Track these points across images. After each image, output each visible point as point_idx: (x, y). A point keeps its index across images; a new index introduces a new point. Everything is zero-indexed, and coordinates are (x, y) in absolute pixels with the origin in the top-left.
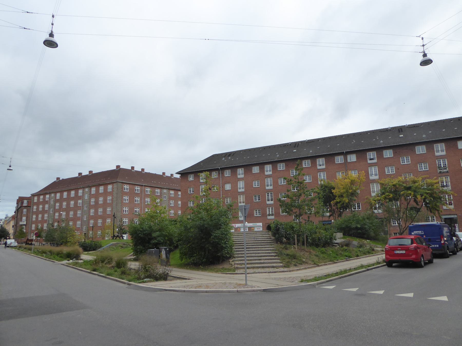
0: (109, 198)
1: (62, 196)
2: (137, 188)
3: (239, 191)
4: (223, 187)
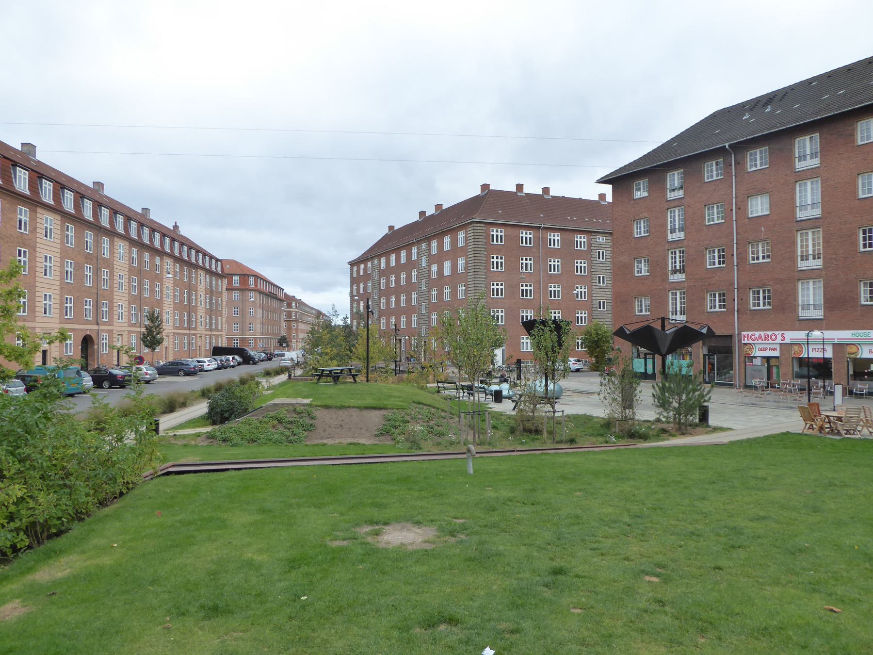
0: (461, 262)
2: (526, 234)
3: (801, 215)
4: (742, 208)
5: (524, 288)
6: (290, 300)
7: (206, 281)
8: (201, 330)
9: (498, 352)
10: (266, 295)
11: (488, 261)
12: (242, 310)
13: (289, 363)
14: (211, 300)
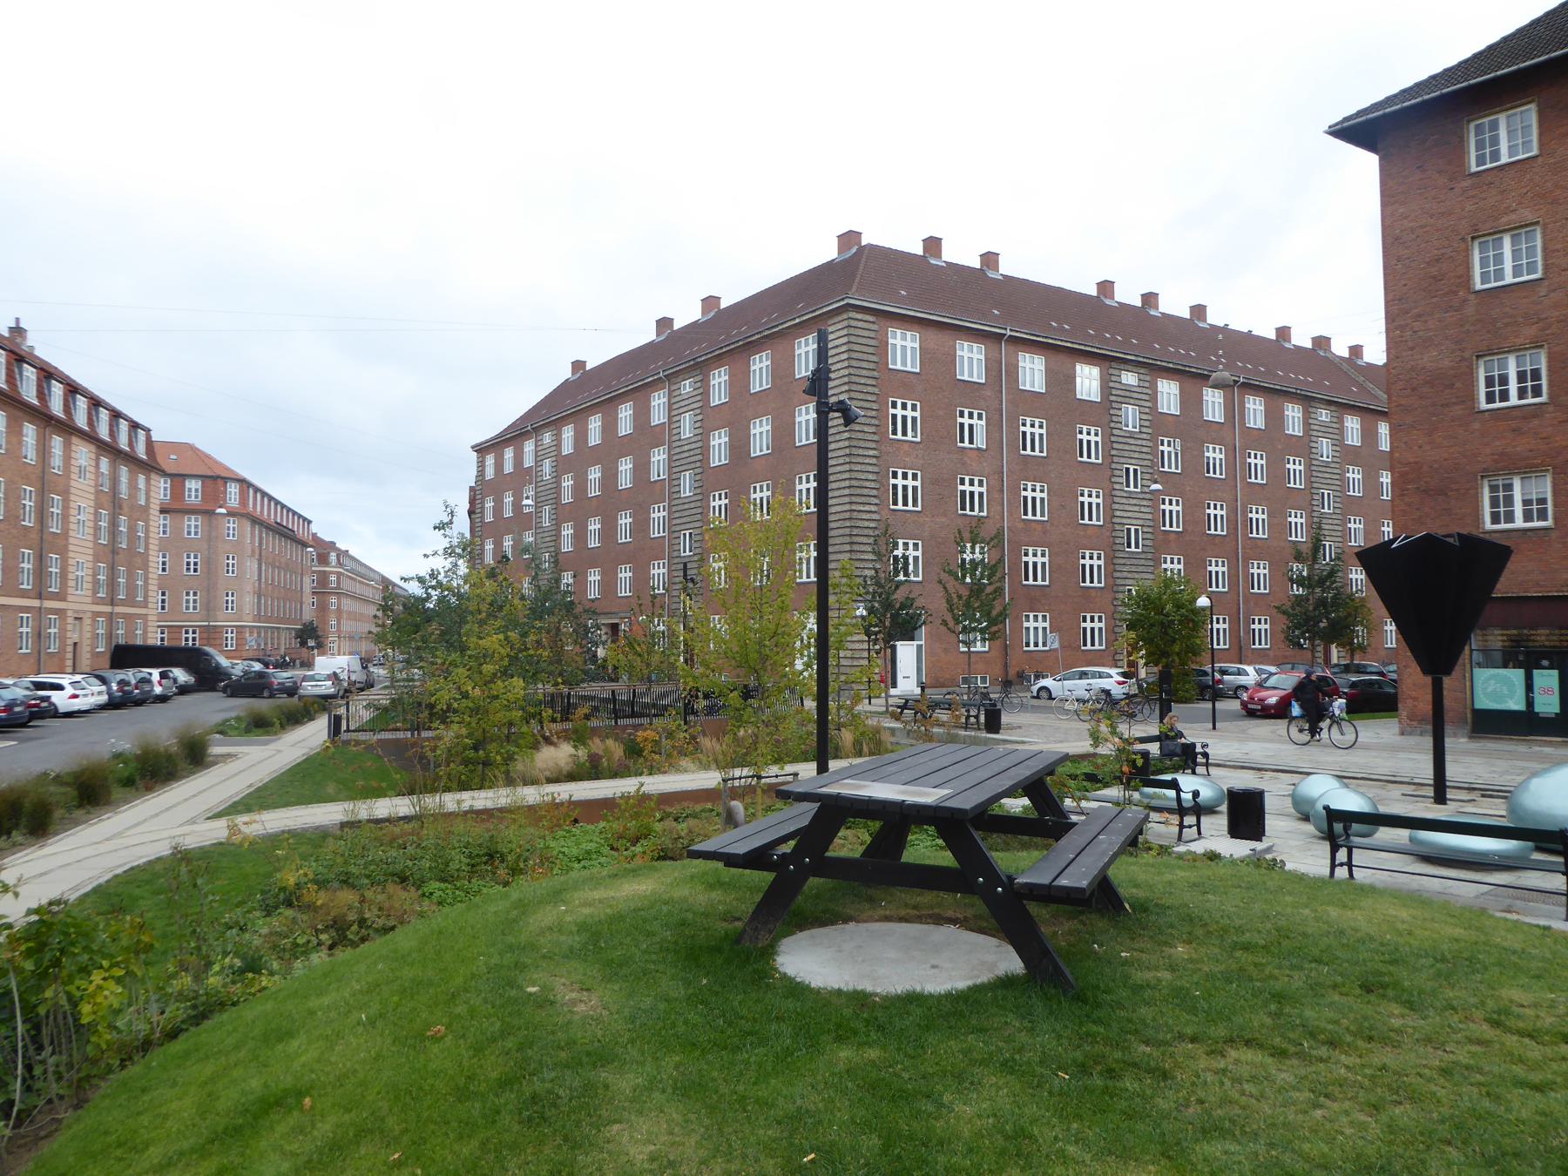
5: (967, 488)
6: (325, 549)
7: (98, 473)
8: (80, 599)
9: (906, 653)
10: (268, 527)
11: (882, 412)
12: (208, 562)
13: (327, 688)
14: (114, 524)
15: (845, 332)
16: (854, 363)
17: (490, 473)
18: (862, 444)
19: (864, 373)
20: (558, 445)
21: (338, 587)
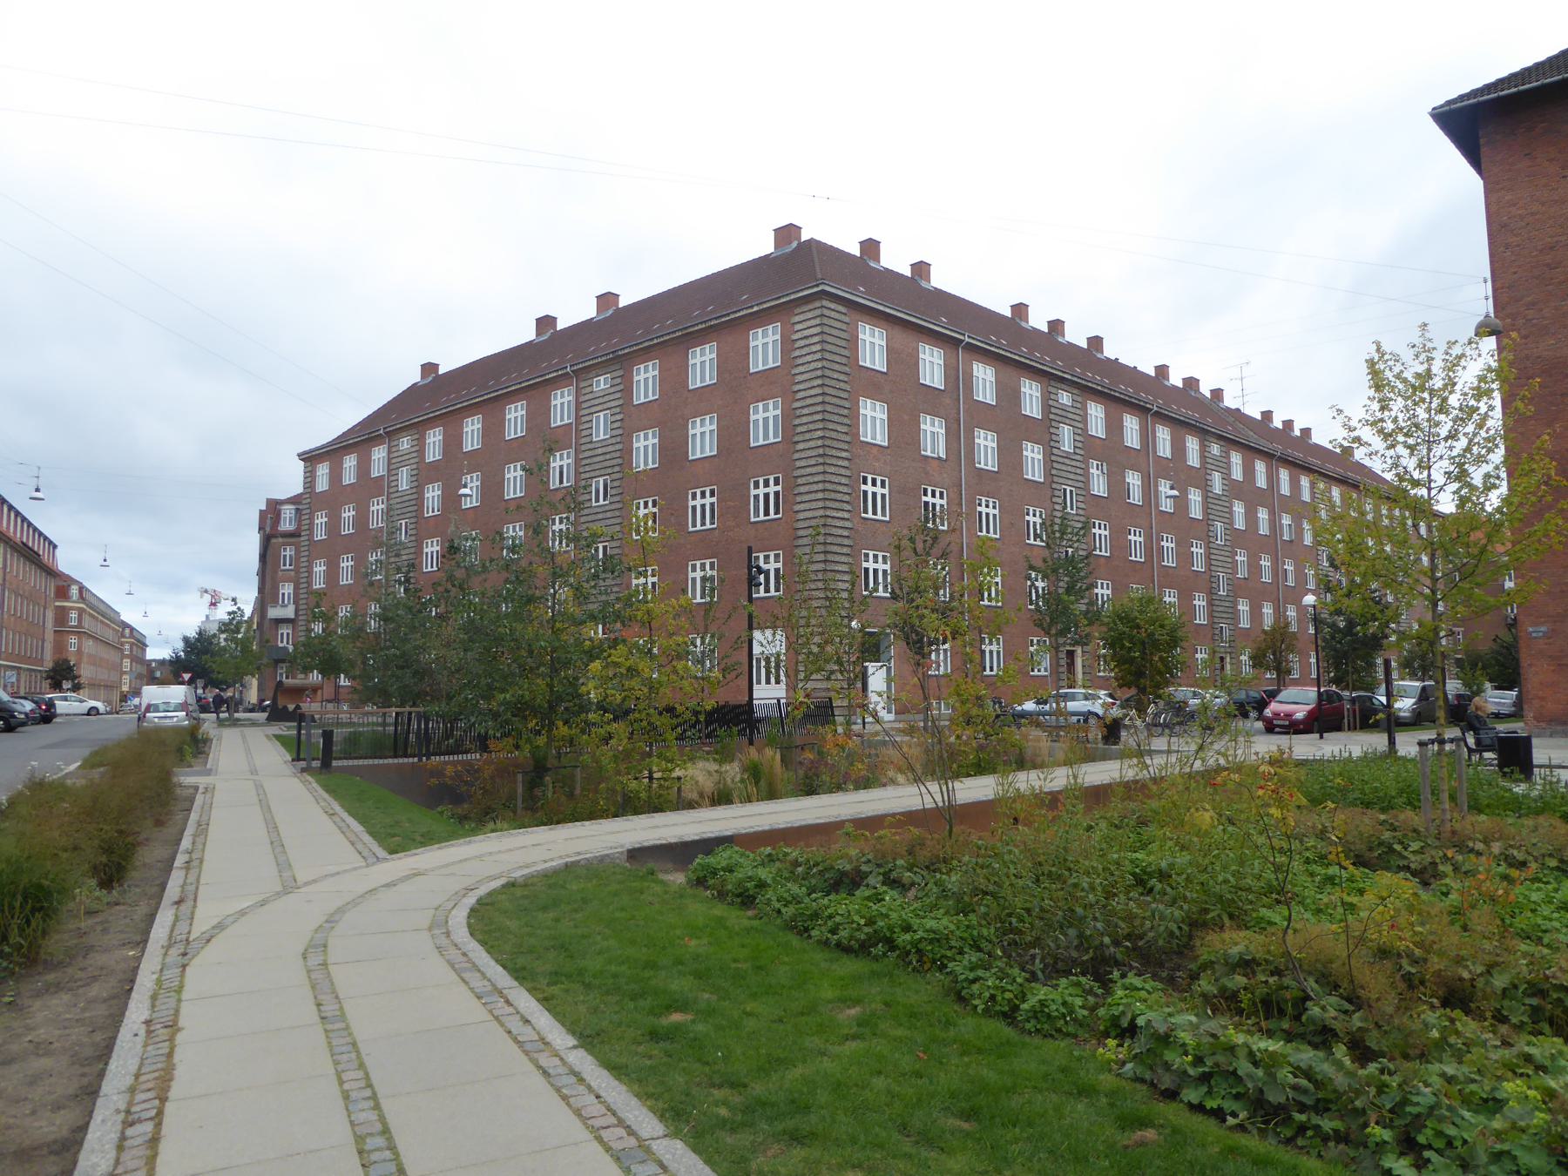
1: (453, 442)
5: (929, 498)
15: (817, 321)
16: (827, 356)
17: (322, 485)
18: (835, 444)
19: (837, 367)
20: (421, 450)
21: (80, 625)
